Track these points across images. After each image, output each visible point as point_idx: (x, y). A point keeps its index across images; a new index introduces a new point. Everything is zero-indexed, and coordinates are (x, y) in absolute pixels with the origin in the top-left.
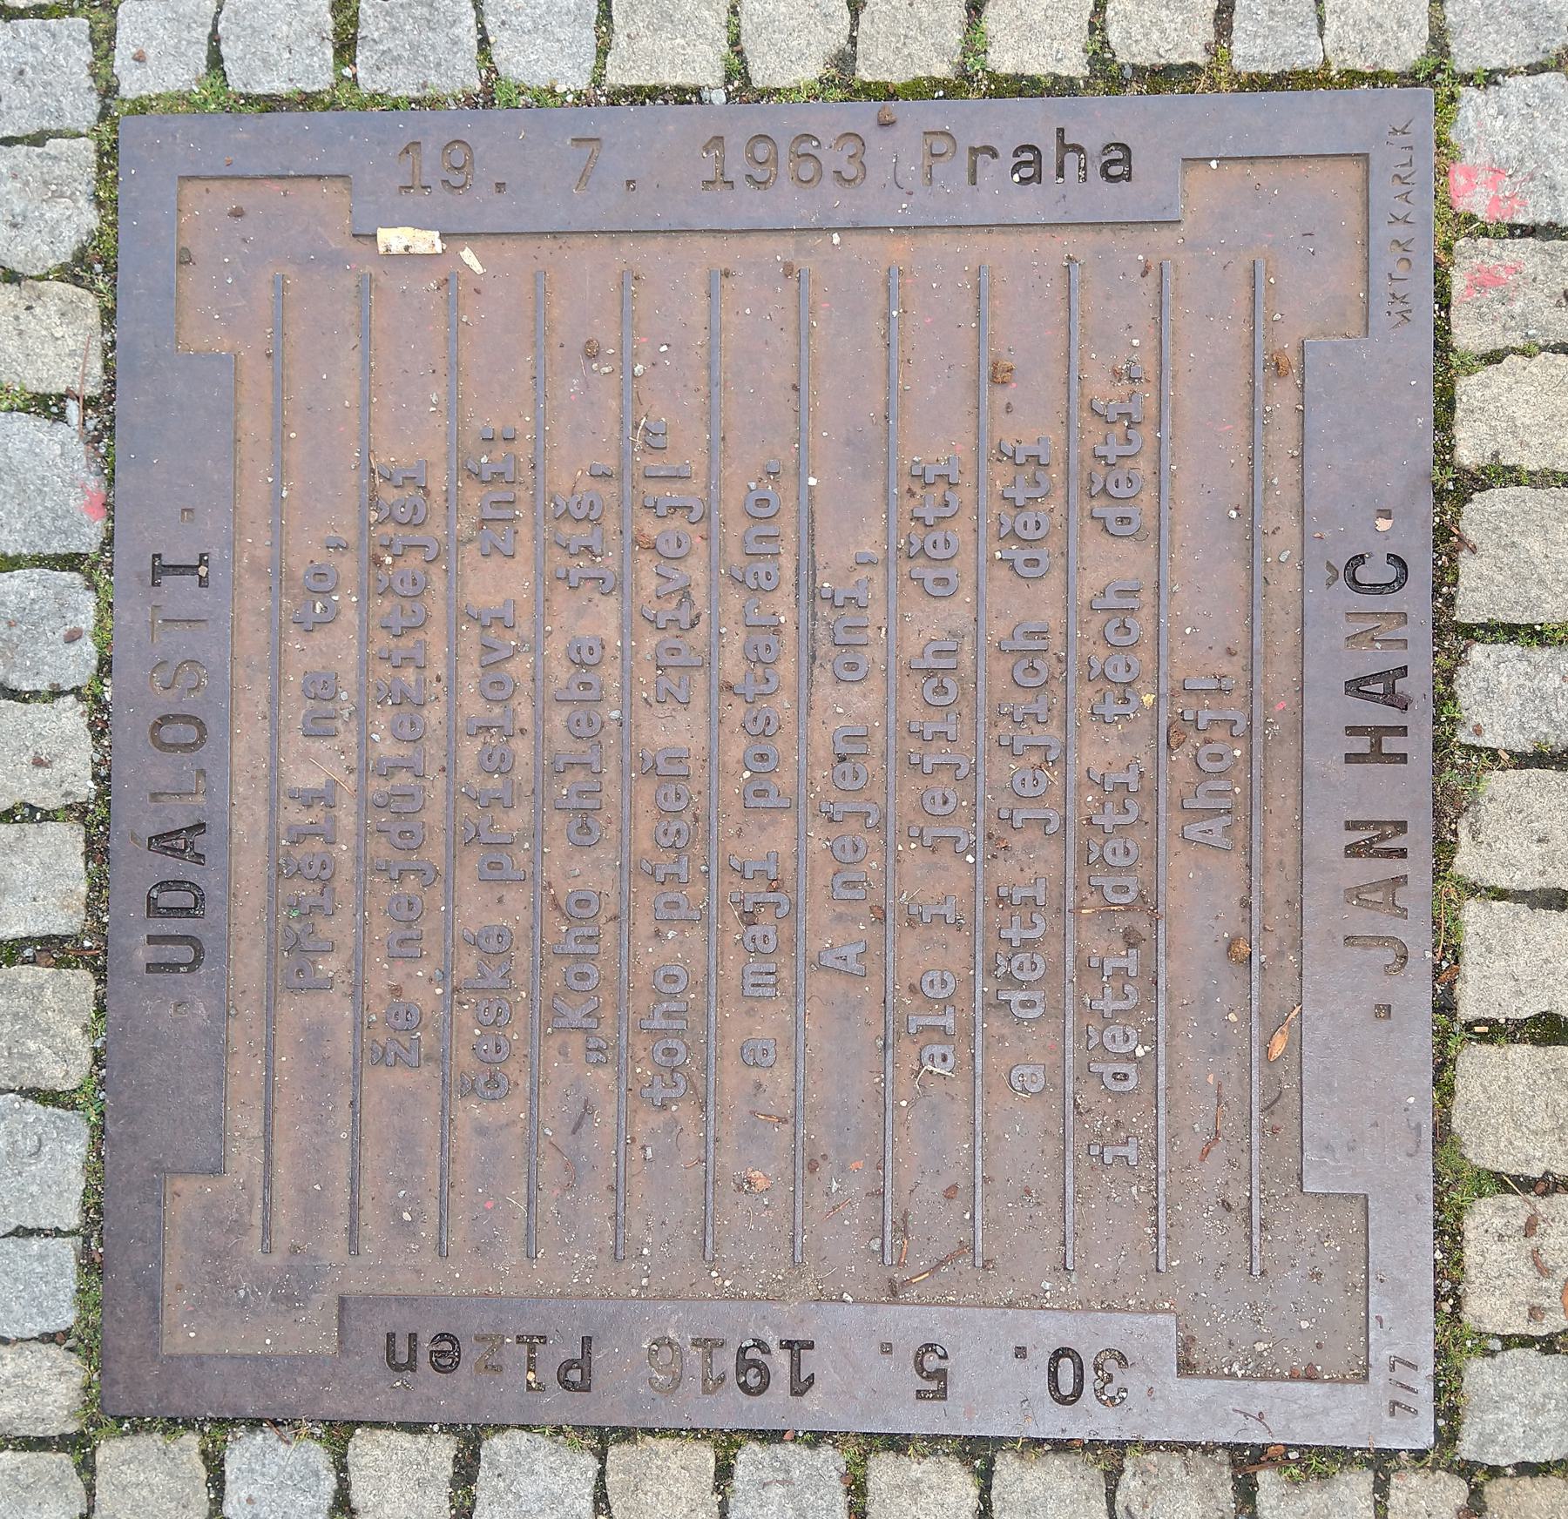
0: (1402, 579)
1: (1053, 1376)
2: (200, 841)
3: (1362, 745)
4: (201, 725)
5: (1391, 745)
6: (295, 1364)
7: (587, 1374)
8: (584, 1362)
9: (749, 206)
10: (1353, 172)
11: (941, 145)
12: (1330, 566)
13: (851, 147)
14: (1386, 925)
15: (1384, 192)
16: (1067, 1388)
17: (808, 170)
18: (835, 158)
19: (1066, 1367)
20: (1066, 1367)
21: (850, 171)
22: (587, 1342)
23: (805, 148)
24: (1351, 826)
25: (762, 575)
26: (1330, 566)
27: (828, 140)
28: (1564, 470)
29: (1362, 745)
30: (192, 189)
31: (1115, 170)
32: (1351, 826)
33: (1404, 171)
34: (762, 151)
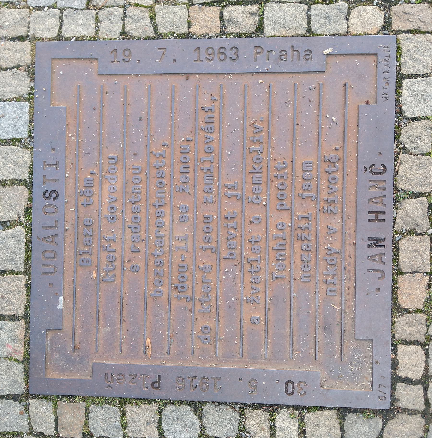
0: (385, 171)
1: (286, 388)
2: (56, 239)
3: (373, 216)
4: (291, 394)
5: (381, 217)
6: (82, 382)
7: (159, 385)
8: (159, 382)
9: (205, 66)
10: (374, 58)
11: (259, 50)
12: (365, 167)
13: (234, 50)
14: (378, 266)
15: (382, 67)
16: (290, 391)
17: (222, 57)
18: (229, 54)
19: (290, 386)
20: (290, 386)
21: (234, 57)
22: (159, 376)
23: (222, 50)
24: (369, 239)
25: (256, 249)
26: (365, 167)
27: (228, 48)
28: (384, 437)
29: (373, 216)
30: (55, 62)
31: (307, 57)
32: (369, 239)
33: (387, 58)
34: (210, 51)
